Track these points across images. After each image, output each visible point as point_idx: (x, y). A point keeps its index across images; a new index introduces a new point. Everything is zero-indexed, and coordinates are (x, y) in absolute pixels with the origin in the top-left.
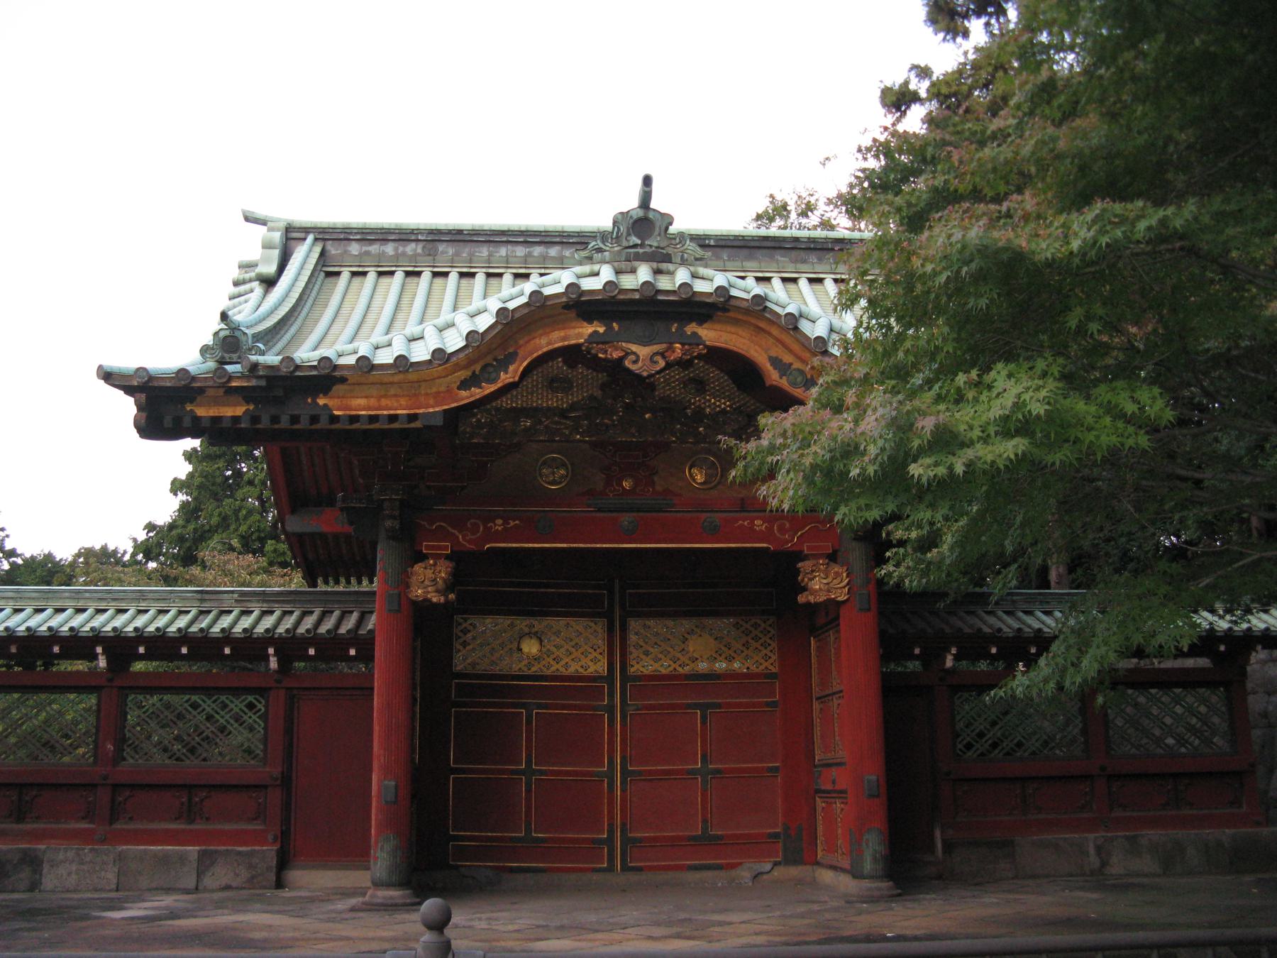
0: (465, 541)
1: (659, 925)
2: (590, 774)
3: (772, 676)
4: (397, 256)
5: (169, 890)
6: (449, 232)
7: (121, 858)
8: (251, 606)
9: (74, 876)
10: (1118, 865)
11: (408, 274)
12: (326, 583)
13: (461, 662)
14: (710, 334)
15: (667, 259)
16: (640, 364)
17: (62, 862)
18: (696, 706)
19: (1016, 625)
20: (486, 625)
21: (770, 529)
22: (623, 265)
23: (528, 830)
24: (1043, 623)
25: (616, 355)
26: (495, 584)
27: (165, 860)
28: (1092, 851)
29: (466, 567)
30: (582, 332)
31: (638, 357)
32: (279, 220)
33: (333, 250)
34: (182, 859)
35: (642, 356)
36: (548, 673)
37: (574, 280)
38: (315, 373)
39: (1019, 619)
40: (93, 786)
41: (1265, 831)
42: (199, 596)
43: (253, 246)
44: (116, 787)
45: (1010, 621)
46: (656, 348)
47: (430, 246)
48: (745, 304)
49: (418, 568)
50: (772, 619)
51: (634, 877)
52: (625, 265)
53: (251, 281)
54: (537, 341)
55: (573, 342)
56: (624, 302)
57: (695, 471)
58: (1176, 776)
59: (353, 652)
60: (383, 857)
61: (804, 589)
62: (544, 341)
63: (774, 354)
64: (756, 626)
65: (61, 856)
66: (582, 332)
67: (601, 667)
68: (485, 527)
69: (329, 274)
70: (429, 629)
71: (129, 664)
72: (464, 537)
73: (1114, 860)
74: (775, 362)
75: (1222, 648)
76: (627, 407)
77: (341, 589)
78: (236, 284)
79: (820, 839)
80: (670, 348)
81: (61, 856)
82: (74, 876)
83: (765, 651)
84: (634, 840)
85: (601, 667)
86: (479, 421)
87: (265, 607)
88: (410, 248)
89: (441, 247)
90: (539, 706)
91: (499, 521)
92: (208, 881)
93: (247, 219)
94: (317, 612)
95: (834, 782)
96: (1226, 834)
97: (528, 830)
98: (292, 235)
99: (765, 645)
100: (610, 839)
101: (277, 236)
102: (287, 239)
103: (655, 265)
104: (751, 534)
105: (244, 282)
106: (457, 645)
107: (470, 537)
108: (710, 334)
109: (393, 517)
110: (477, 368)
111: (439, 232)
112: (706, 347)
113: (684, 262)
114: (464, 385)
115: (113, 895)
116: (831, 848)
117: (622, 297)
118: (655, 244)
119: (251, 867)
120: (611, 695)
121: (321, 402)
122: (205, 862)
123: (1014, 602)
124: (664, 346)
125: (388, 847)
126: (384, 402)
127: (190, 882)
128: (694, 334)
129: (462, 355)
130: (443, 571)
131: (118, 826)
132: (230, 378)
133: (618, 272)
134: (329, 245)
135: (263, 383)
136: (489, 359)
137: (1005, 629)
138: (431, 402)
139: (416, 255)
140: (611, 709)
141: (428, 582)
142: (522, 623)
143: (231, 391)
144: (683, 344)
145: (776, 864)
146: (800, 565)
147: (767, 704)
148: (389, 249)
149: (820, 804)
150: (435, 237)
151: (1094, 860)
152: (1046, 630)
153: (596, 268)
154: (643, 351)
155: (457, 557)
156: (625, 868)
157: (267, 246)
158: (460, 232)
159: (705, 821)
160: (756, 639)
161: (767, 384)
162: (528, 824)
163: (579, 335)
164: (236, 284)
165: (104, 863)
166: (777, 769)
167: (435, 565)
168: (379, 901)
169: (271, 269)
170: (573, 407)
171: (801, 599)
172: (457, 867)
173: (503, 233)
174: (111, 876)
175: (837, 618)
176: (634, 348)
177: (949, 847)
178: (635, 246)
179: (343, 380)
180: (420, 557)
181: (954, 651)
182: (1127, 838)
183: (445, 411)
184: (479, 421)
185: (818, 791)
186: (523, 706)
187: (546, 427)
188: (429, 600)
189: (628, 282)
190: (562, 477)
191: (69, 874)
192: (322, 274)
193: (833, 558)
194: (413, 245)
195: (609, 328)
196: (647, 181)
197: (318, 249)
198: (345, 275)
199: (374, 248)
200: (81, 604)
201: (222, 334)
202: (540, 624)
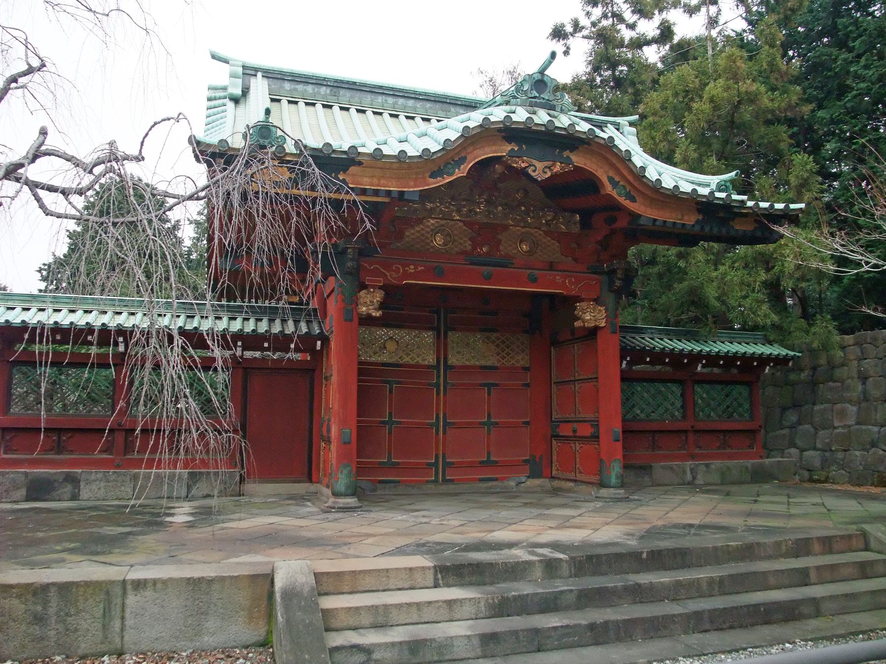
0: (392, 277)
4: (314, 94)
6: (348, 82)
9: (102, 490)
10: (700, 480)
14: (578, 159)
16: (537, 173)
17: (94, 481)
18: (484, 385)
25: (523, 165)
28: (688, 472)
30: (504, 149)
38: (345, 156)
45: (679, 343)
47: (335, 90)
49: (363, 293)
53: (225, 98)
63: (610, 175)
64: (498, 339)
65: (93, 477)
66: (504, 149)
68: (404, 270)
72: (390, 275)
73: (699, 476)
74: (611, 180)
81: (93, 477)
82: (102, 490)
89: (342, 92)
90: (398, 383)
91: (412, 267)
92: (194, 491)
93: (214, 57)
96: (749, 463)
97: (390, 458)
99: (523, 351)
100: (436, 463)
107: (395, 275)
108: (578, 159)
109: (351, 260)
111: (342, 82)
112: (575, 166)
118: (547, 98)
120: (438, 377)
124: (551, 163)
125: (345, 472)
126: (382, 181)
127: (183, 493)
128: (568, 157)
130: (379, 296)
138: (412, 184)
139: (326, 95)
140: (437, 385)
150: (339, 85)
151: (689, 477)
154: (540, 165)
155: (389, 290)
156: (445, 481)
157: (233, 76)
158: (354, 83)
161: (602, 192)
162: (390, 454)
165: (123, 481)
168: (341, 506)
169: (238, 92)
179: (360, 163)
180: (363, 287)
186: (388, 382)
191: (99, 489)
193: (597, 301)
194: (324, 88)
195: (520, 148)
199: (300, 87)
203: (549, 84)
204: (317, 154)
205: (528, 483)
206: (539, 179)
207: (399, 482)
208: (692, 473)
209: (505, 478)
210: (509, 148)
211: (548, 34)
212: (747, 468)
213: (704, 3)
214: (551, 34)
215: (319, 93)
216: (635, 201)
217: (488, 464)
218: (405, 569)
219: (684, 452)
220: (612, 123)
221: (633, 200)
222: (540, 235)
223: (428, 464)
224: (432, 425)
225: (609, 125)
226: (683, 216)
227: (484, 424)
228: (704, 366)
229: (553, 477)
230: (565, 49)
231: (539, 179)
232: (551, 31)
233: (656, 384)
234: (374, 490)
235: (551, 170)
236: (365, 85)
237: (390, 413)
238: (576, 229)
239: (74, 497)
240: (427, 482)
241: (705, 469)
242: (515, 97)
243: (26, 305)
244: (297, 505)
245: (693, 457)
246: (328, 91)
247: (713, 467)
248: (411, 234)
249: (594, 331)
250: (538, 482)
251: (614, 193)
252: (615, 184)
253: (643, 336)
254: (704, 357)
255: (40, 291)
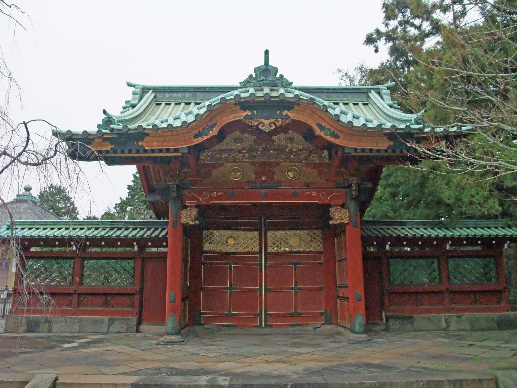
0: (203, 201)
1: (272, 354)
2: (253, 289)
3: (321, 252)
4: (182, 98)
5: (97, 333)
6: (201, 88)
7: (80, 320)
8: (128, 227)
10: (453, 327)
11: (186, 104)
12: (164, 219)
13: (206, 247)
15: (276, 85)
16: (265, 127)
19: (413, 233)
20: (219, 234)
21: (318, 196)
22: (258, 88)
23: (230, 311)
24: (423, 232)
26: (214, 217)
27: (95, 322)
29: (203, 211)
31: (264, 124)
32: (140, 85)
33: (159, 96)
34: (102, 321)
35: (266, 125)
36: (238, 251)
37: (239, 93)
39: (414, 231)
40: (70, 294)
41: (511, 314)
42: (110, 223)
43: (128, 94)
44: (80, 294)
46: (271, 121)
47: (194, 93)
48: (306, 102)
50: (320, 231)
51: (268, 330)
52: (259, 87)
54: (224, 118)
55: (238, 119)
56: (258, 102)
57: (290, 173)
58: (475, 292)
59: (103, 243)
60: (170, 323)
61: (331, 219)
62: (227, 119)
67: (257, 249)
69: (157, 104)
70: (192, 235)
71: (144, 249)
73: (452, 324)
74: (319, 125)
75: (494, 242)
76: (264, 149)
77: (166, 220)
78: (124, 108)
79: (339, 315)
80: (277, 121)
81: (59, 320)
83: (318, 243)
84: (270, 314)
85: (257, 249)
86: (207, 154)
87: (134, 227)
88: (187, 95)
89: (198, 94)
90: (234, 264)
91: (215, 193)
92: (112, 329)
94: (153, 229)
95: (344, 294)
96: (496, 315)
97: (230, 311)
98: (145, 90)
99: (318, 241)
101: (138, 90)
102: (143, 92)
103: (271, 88)
104: (311, 197)
105: (127, 107)
106: (204, 241)
110: (201, 129)
111: (198, 88)
112: (291, 120)
113: (282, 86)
114: (196, 136)
115: (77, 334)
116: (343, 318)
117: (256, 99)
118: (271, 79)
119: (127, 324)
121: (140, 144)
122: (111, 322)
123: (412, 225)
125: (171, 319)
126: (165, 144)
128: (286, 115)
129: (194, 124)
130: (194, 212)
131: (80, 309)
132: (104, 134)
133: (256, 91)
134: (158, 94)
135: (116, 136)
136: (205, 126)
137: (409, 235)
138: (183, 143)
139: (189, 97)
140: (260, 265)
141: (189, 217)
142: (229, 233)
143: (105, 140)
144: (282, 119)
145: (323, 324)
146: (330, 209)
147: (319, 263)
148: (180, 95)
149: (339, 301)
151: (444, 325)
152: (425, 235)
153: (247, 89)
154: (267, 122)
156: (266, 326)
157: (134, 94)
158: (205, 88)
159: (296, 308)
160: (315, 239)
163: (241, 116)
164: (124, 108)
166: (323, 288)
167: (190, 210)
168: (168, 340)
170: (243, 149)
171: (331, 222)
172: (204, 324)
173: (221, 88)
174: (76, 327)
175: (344, 231)
176: (263, 120)
177: (387, 318)
178: (263, 80)
179: (148, 135)
180: (186, 207)
181: (389, 243)
182: (456, 316)
183: (188, 147)
184: (207, 154)
185: (338, 297)
186: (228, 264)
187: (233, 156)
188: (189, 223)
189: (260, 94)
190: (240, 176)
191: (62, 326)
192: (155, 104)
193: (343, 206)
194: (188, 94)
196: (267, 52)
197: (153, 95)
198: (163, 104)
199: (174, 95)
200: (68, 227)
201: (105, 120)
202: (235, 233)
203: (272, 71)
204: (120, 132)
205: (322, 328)
206: (267, 131)
207: (233, 326)
208: (446, 322)
209: (307, 325)
210: (245, 114)
211: (363, 42)
212: (493, 319)
213: (454, 3)
214: (365, 42)
215: (185, 97)
216: (339, 138)
217: (296, 315)
218: (112, 384)
219: (442, 306)
220: (374, 89)
221: (337, 137)
222: (302, 166)
223: (255, 315)
224: (257, 290)
225: (372, 91)
226: (377, 143)
227: (292, 289)
228: (451, 245)
229: (338, 325)
230: (375, 49)
231: (267, 131)
232: (365, 39)
233: (457, 259)
234: (219, 331)
235: (274, 124)
236: (328, 89)
237: (230, 283)
238: (326, 161)
239: (49, 331)
240: (255, 326)
241: (457, 319)
242: (249, 82)
243: (30, 227)
244: (375, 335)
245: (449, 310)
246: (190, 95)
247: (464, 318)
248: (215, 173)
249: (342, 226)
250: (329, 327)
251: (322, 134)
252: (322, 128)
253: (403, 227)
254: (508, 239)
255: (84, 219)
